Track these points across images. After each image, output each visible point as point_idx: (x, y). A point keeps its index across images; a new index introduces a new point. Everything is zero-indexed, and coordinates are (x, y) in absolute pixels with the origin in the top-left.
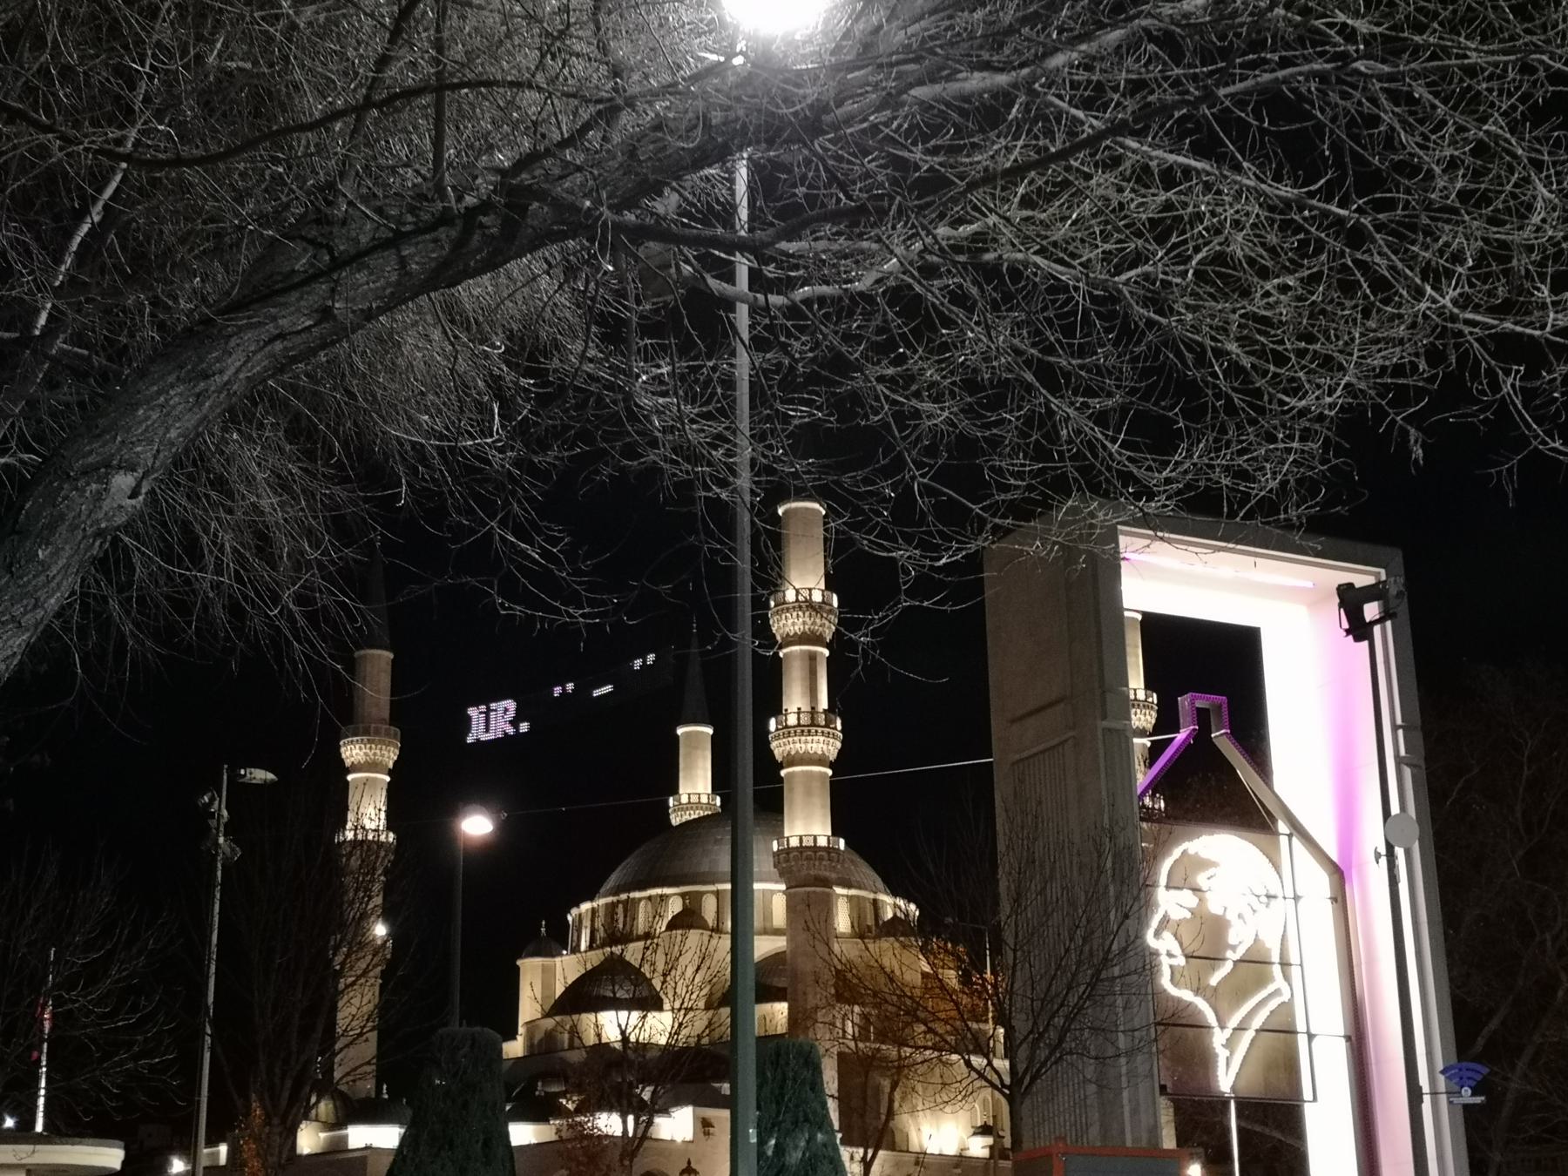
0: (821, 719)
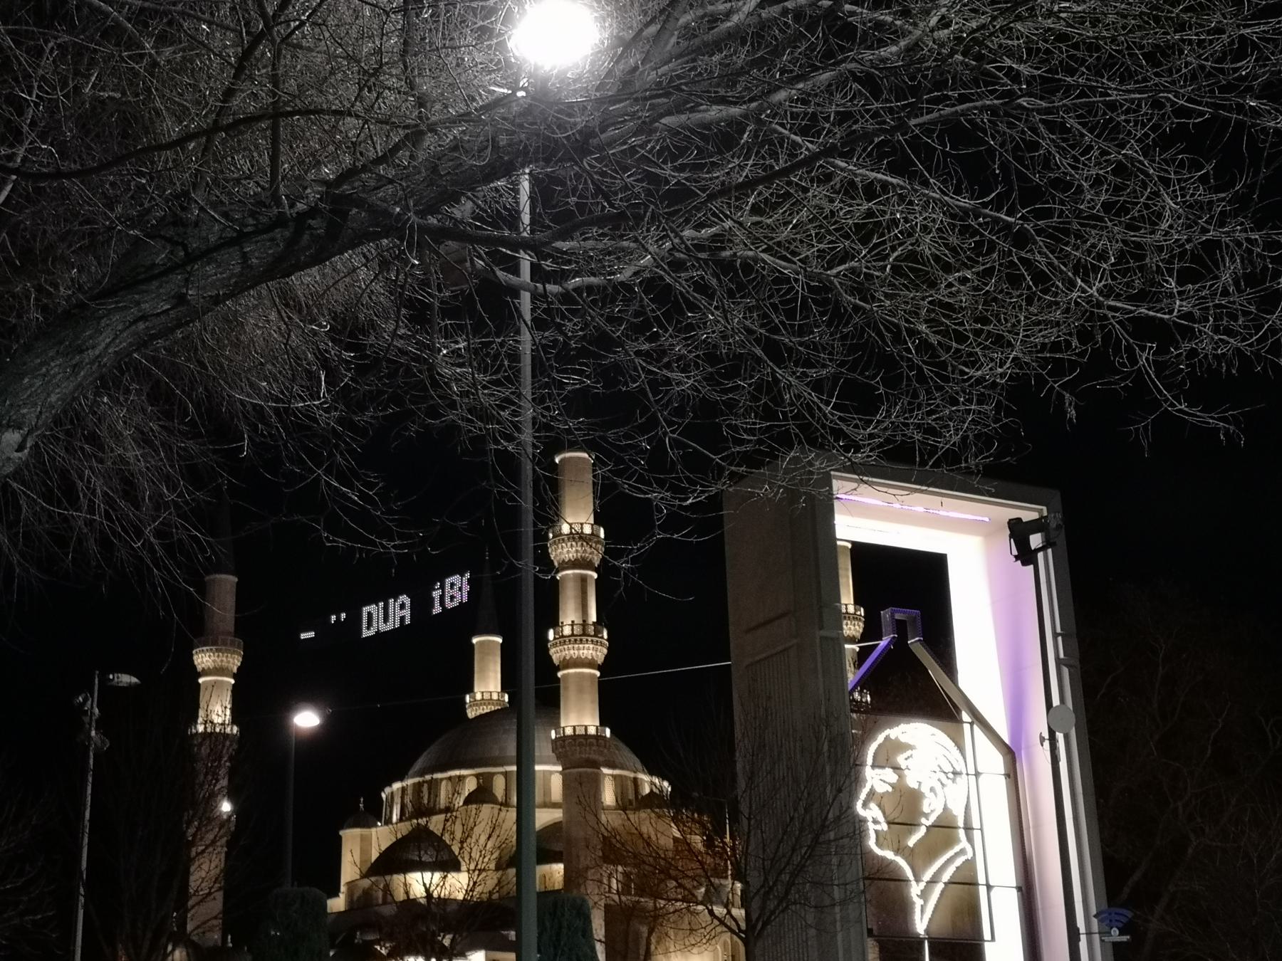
0: (591, 630)
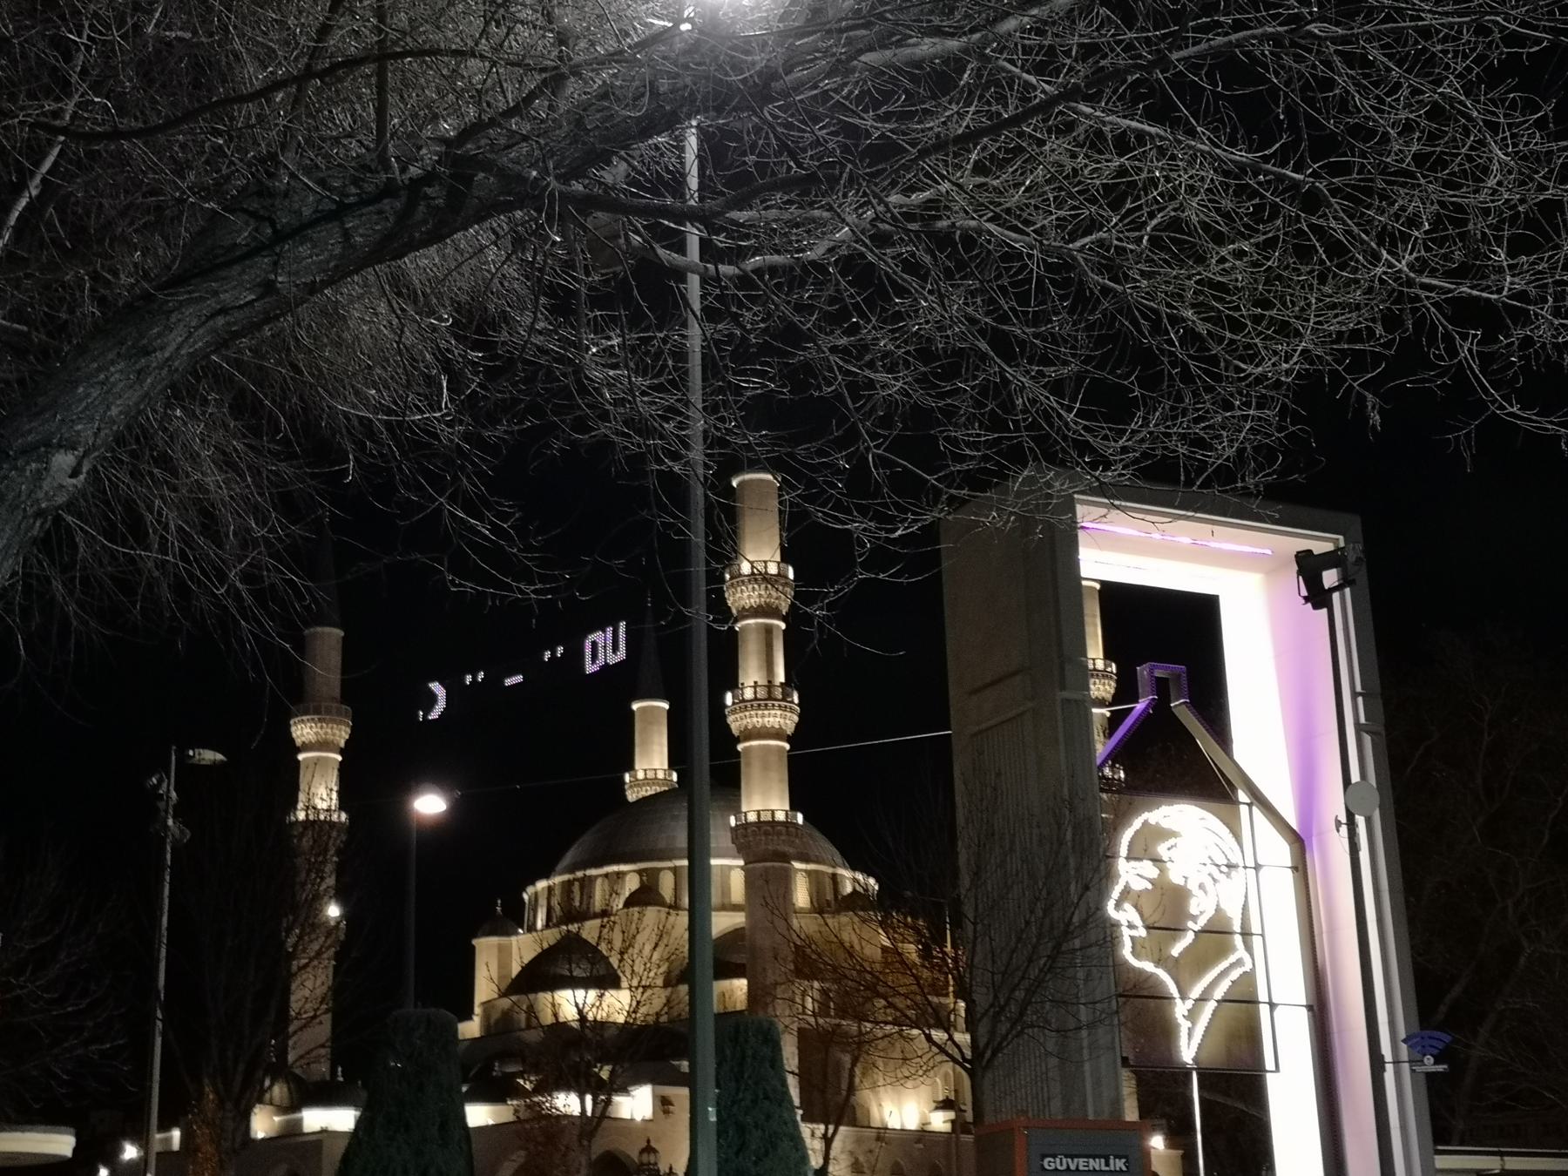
0: (778, 693)
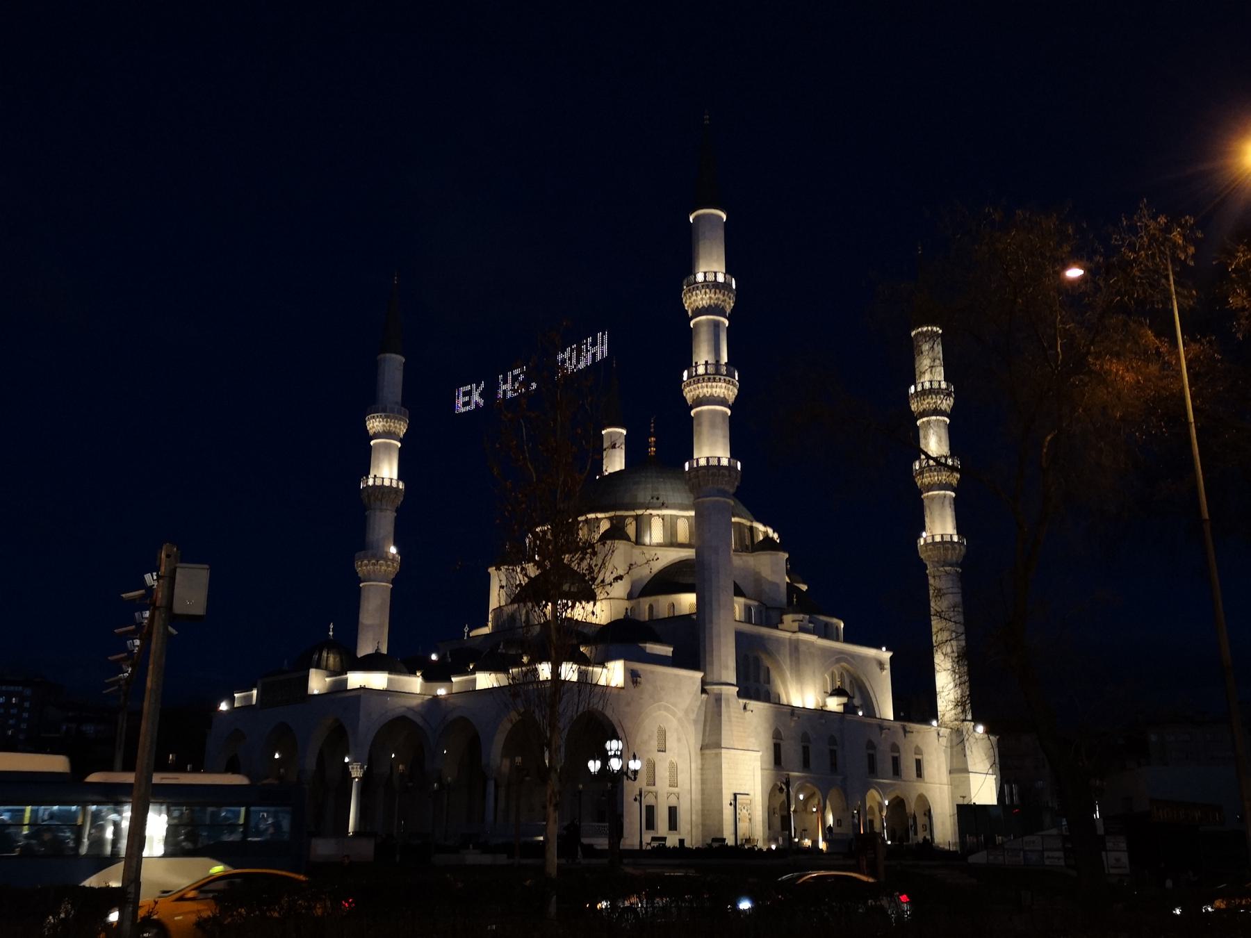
0: (724, 370)
